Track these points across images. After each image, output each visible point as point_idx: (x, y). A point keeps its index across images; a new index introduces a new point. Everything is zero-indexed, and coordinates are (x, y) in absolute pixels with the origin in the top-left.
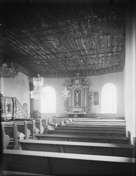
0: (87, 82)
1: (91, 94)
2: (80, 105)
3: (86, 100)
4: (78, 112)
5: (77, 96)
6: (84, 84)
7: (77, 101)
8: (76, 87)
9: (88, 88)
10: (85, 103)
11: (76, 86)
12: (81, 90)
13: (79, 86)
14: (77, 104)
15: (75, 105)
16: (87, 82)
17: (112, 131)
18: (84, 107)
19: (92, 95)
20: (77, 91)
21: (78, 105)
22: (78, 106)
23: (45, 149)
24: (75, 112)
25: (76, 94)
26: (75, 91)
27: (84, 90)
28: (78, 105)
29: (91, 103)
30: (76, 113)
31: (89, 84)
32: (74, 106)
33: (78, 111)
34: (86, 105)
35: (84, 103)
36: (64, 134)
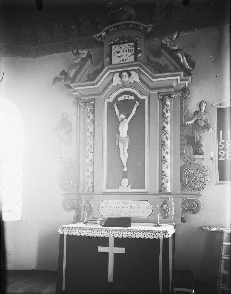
0: (178, 50)
1: (202, 124)
2: (138, 182)
3: (173, 154)
4: (125, 222)
5: (124, 129)
6: (158, 64)
7: (124, 158)
8: (118, 87)
9: (185, 91)
10: (168, 172)
11: (116, 80)
12: (142, 102)
13: (135, 77)
14: (125, 175)
15: (114, 183)
16: (178, 50)
17: (170, 62)
18: (162, 189)
19: (207, 127)
20: (125, 107)
21: (125, 182)
22: (129, 190)
23: (148, 71)
24: (112, 222)
25: (118, 123)
26: (111, 105)
27: (163, 102)
28: (125, 182)
29: (200, 168)
30: (112, 233)
31: (192, 64)
32: (105, 189)
33: (123, 215)
34: (173, 187)
35: (162, 173)
36: (146, 87)
